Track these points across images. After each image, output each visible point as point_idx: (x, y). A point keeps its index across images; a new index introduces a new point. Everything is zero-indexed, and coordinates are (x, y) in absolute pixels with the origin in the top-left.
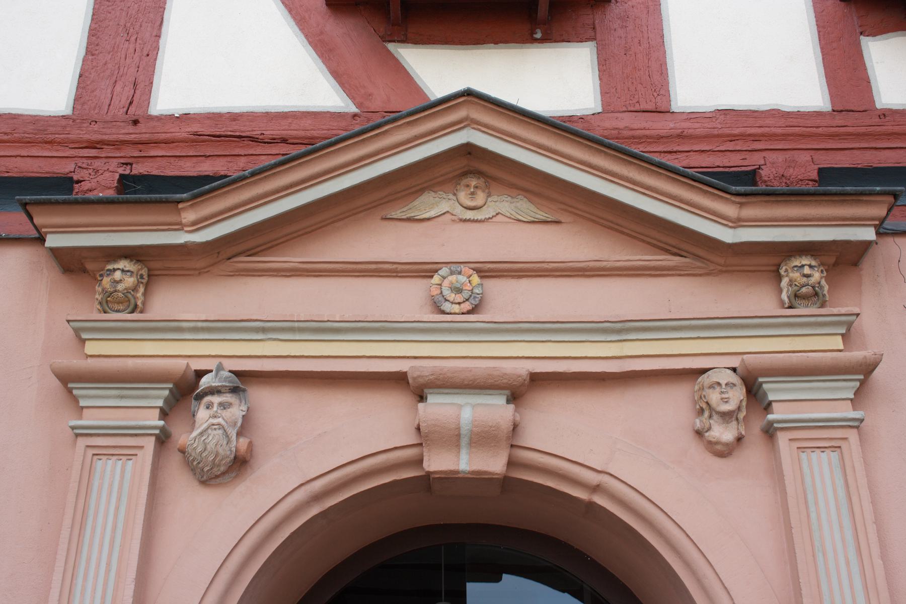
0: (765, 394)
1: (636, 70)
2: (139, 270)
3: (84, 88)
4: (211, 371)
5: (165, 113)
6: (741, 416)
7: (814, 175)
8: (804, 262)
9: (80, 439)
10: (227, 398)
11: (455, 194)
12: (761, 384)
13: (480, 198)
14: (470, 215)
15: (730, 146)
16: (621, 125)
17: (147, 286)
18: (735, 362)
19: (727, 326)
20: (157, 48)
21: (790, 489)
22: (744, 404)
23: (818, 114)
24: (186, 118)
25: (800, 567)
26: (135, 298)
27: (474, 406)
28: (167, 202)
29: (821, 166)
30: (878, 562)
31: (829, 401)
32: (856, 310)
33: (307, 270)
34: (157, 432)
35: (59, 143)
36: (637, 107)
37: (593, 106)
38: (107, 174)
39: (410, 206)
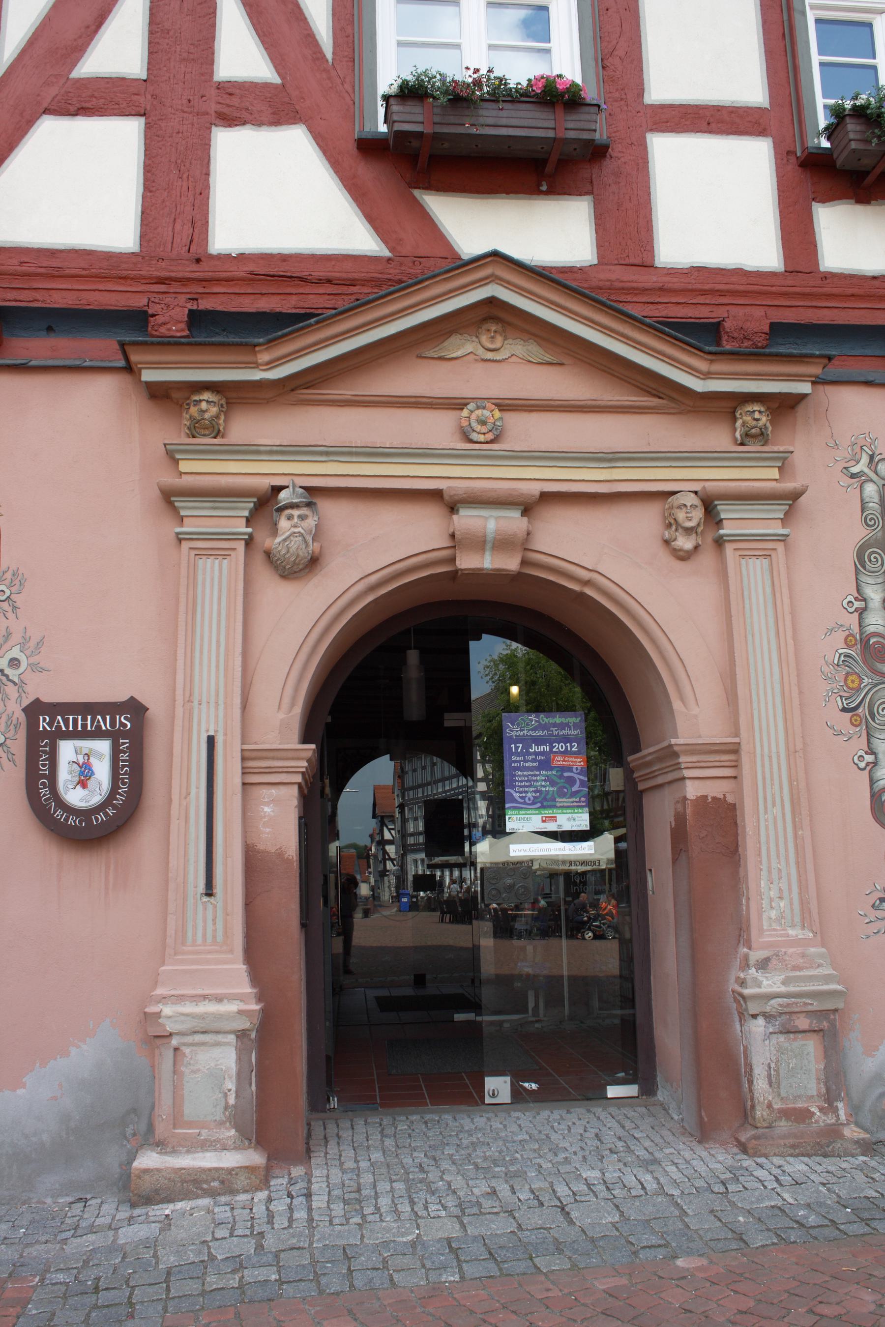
0: (718, 513)
1: (626, 223)
2: (219, 400)
3: (147, 225)
4: (287, 487)
5: (223, 252)
6: (700, 530)
7: (766, 329)
8: (755, 409)
10: (304, 511)
11: (477, 337)
12: (716, 506)
13: (498, 343)
14: (490, 355)
15: (701, 299)
16: (613, 277)
17: (226, 414)
18: (697, 487)
19: (695, 458)
20: (208, 187)
21: (732, 588)
23: (773, 274)
24: (242, 257)
25: (736, 645)
26: (218, 424)
27: (497, 518)
28: (246, 344)
30: (790, 642)
31: (762, 521)
32: (791, 449)
33: (358, 402)
34: (246, 537)
35: (132, 279)
36: (627, 261)
37: (590, 258)
38: (178, 309)
39: (441, 346)
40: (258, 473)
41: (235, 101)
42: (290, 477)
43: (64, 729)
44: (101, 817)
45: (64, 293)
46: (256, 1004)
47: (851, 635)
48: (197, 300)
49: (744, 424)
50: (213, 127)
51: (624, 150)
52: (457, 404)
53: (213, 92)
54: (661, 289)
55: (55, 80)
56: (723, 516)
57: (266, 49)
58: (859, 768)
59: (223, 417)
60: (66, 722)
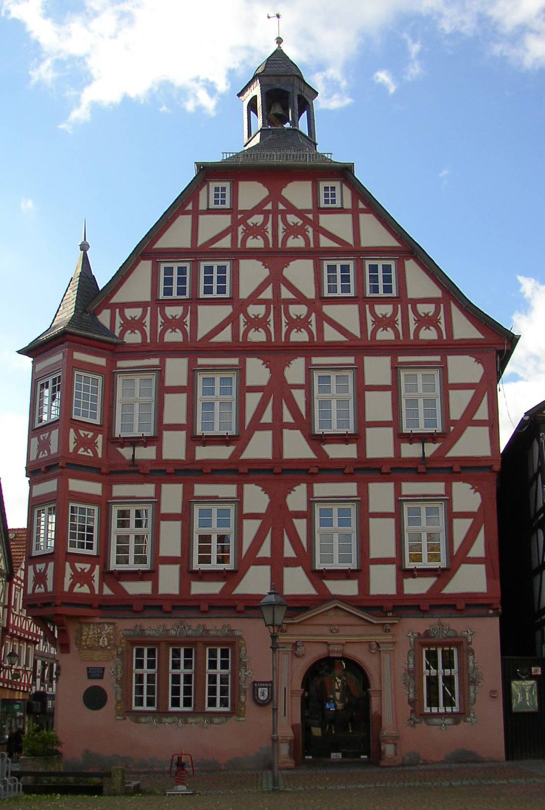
1: (364, 586)
40: (293, 639)
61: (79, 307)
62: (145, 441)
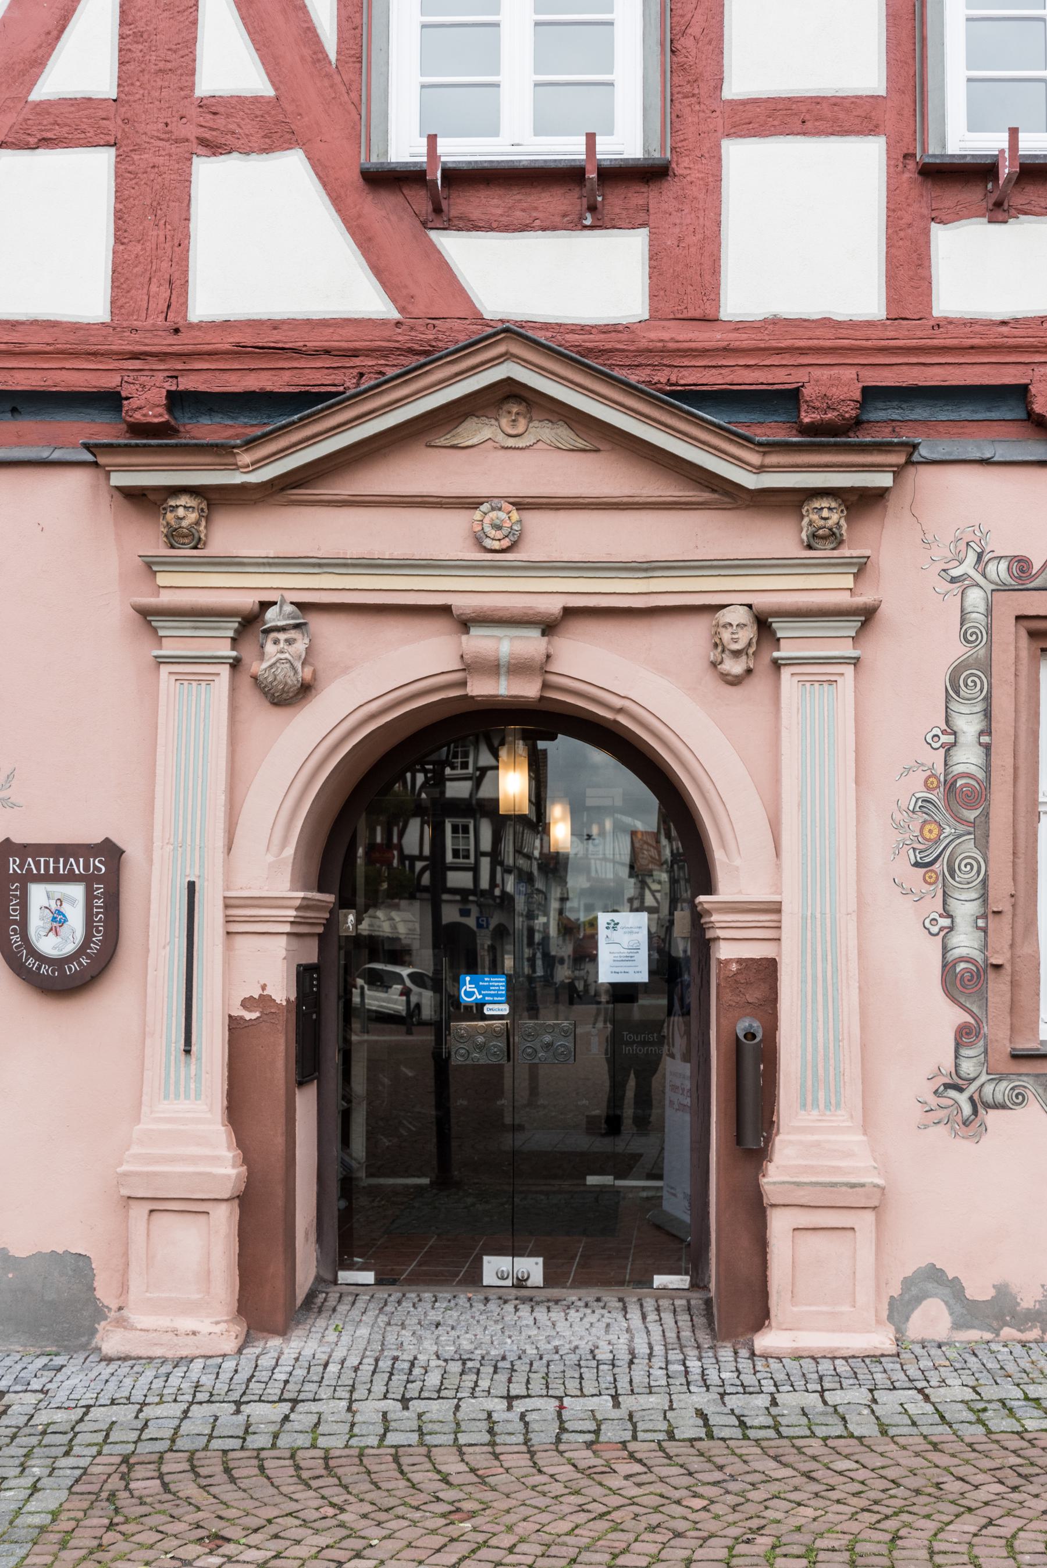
1: (686, 272)
2: (199, 504)
3: (118, 287)
4: (275, 603)
6: (751, 651)
7: (857, 395)
8: (823, 505)
9: (162, 666)
10: (292, 634)
11: (497, 420)
13: (522, 423)
14: (511, 442)
15: (775, 360)
16: (666, 335)
22: (754, 640)
24: (226, 326)
26: (198, 531)
29: (866, 384)
34: (231, 661)
35: (102, 355)
38: (155, 390)
39: (454, 432)
40: (238, 591)
41: (220, 122)
42: (280, 592)
43: (35, 872)
44: (74, 967)
45: (27, 374)
46: (234, 1167)
47: (933, 775)
48: (176, 377)
49: (810, 523)
50: (194, 156)
51: (692, 166)
52: (471, 503)
53: (193, 112)
54: (725, 349)
55: (12, 105)
56: (779, 635)
57: (257, 50)
58: (930, 933)
59: (203, 523)
60: (37, 864)
61: (257, 46)
62: (585, 191)
